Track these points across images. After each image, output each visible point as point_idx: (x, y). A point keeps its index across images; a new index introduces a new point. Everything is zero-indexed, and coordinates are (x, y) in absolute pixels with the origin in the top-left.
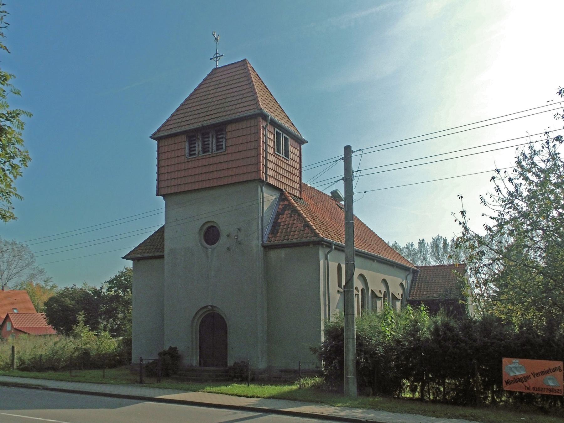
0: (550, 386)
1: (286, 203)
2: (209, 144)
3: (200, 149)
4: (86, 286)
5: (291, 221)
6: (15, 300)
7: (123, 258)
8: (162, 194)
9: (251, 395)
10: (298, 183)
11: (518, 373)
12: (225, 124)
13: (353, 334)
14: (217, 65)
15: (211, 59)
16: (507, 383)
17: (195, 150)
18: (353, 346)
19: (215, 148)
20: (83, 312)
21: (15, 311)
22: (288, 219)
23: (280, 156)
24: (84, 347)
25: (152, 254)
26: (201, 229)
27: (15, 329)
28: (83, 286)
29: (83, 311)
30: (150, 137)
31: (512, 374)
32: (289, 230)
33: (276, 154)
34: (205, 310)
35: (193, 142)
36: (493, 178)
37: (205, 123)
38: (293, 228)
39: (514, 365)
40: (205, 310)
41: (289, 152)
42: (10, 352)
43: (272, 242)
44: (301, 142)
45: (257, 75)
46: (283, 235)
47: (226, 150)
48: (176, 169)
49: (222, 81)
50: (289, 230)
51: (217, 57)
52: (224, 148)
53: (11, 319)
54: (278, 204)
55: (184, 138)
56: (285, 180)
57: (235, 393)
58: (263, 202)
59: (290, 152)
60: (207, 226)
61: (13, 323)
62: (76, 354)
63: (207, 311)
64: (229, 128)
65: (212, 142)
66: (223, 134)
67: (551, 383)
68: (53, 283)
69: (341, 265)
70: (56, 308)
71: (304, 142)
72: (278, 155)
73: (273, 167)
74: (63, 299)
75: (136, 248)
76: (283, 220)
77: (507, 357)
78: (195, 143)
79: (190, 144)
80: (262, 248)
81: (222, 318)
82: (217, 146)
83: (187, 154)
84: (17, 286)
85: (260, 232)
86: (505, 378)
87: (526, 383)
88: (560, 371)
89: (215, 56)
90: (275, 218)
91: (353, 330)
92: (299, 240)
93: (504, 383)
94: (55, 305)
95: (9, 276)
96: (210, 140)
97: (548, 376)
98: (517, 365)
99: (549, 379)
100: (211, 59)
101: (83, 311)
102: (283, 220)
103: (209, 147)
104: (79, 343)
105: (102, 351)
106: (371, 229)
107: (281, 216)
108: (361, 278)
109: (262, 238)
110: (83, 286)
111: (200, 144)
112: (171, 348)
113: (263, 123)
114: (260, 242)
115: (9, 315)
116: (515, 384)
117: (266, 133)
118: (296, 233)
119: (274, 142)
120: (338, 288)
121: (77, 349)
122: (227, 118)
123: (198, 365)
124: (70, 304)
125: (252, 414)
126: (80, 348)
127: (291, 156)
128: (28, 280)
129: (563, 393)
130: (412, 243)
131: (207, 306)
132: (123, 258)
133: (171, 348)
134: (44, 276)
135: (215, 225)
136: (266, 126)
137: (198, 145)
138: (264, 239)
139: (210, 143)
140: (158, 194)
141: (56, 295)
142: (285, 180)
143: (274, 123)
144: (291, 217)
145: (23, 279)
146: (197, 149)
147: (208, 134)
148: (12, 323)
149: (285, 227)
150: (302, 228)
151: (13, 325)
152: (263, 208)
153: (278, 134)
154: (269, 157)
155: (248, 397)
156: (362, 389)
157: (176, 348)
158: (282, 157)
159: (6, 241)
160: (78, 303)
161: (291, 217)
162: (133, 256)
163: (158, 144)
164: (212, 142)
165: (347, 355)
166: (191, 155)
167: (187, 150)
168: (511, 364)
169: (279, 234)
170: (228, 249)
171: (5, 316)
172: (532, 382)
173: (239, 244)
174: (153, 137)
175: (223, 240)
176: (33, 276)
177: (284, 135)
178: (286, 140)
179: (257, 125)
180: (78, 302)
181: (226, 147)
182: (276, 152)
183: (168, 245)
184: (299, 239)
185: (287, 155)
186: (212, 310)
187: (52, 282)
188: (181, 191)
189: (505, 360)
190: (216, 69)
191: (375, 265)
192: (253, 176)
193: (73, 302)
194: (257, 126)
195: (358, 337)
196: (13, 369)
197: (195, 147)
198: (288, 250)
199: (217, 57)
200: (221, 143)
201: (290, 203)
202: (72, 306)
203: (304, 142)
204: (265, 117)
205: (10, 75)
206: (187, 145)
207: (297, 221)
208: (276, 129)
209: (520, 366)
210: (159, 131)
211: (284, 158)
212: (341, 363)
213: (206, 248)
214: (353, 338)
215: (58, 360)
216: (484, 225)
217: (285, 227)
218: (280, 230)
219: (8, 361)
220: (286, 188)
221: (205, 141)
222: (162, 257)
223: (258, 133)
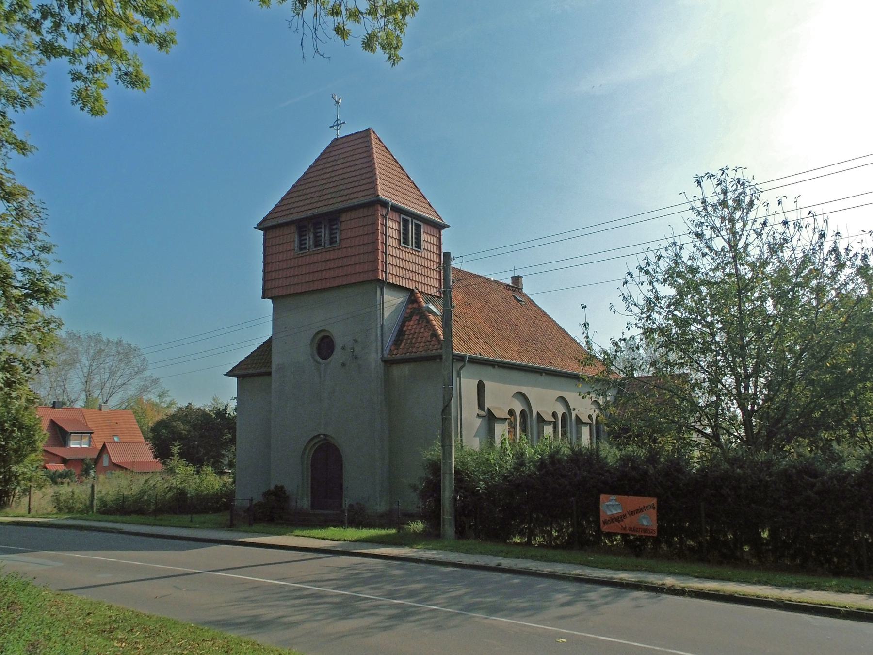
0: (643, 525)
1: (415, 305)
2: (321, 236)
3: (311, 243)
4: (216, 402)
5: (418, 330)
6: (117, 423)
7: (225, 375)
8: (270, 296)
9: (338, 538)
10: (436, 279)
11: (614, 512)
12: (340, 212)
13: (451, 470)
14: (337, 135)
15: (331, 127)
16: (605, 523)
17: (305, 243)
18: (450, 483)
19: (327, 242)
20: (177, 443)
21: (116, 439)
22: (414, 327)
23: (408, 248)
24: (179, 486)
25: (258, 371)
26: (313, 340)
27: (114, 464)
28: (213, 402)
29: (178, 441)
30: (255, 228)
31: (609, 513)
32: (413, 341)
33: (402, 246)
34: (316, 440)
35: (304, 233)
36: (626, 283)
37: (316, 211)
38: (419, 338)
39: (611, 503)
40: (316, 440)
41: (422, 241)
42: (90, 490)
43: (394, 356)
44: (439, 227)
45: (385, 147)
47: (340, 244)
48: (285, 266)
49: (341, 156)
50: (413, 341)
51: (338, 125)
52: (338, 241)
53: (109, 449)
54: (406, 308)
55: (293, 229)
56: (417, 278)
57: (323, 537)
58: (383, 308)
59: (424, 241)
60: (320, 336)
61: (111, 456)
62: (170, 494)
63: (319, 441)
64: (344, 217)
66: (336, 224)
67: (645, 523)
68: (170, 399)
69: (484, 382)
70: (166, 435)
71: (444, 226)
72: (405, 247)
73: (398, 262)
74: (174, 424)
75: (241, 362)
76: (409, 328)
77: (605, 494)
78: (305, 235)
79: (300, 236)
80: (382, 364)
81: (337, 450)
82: (331, 239)
83: (296, 249)
84: (122, 403)
85: (379, 344)
86: (602, 519)
87: (622, 523)
88: (654, 508)
89: (336, 124)
90: (401, 326)
91: (451, 463)
92: (424, 354)
93: (602, 524)
94: (164, 431)
95: (112, 389)
96: (323, 231)
97: (642, 515)
98: (614, 502)
99: (644, 518)
100: (331, 127)
101: (178, 441)
102: (409, 328)
103: (321, 240)
104: (176, 482)
105: (202, 491)
106: (566, 330)
107: (407, 322)
108: (521, 398)
109: (382, 352)
110: (213, 402)
111: (312, 236)
112: (276, 487)
113: (382, 211)
114: (380, 355)
115: (106, 444)
116: (612, 525)
117: (386, 223)
118: (422, 344)
119: (399, 231)
120: (476, 411)
121: (171, 489)
122: (340, 206)
123: (310, 508)
124: (184, 430)
125: (315, 555)
126: (174, 488)
127: (424, 245)
128: (137, 394)
129: (656, 534)
131: (320, 435)
132: (225, 375)
133: (276, 487)
134: (158, 389)
136: (387, 214)
137: (310, 238)
138: (384, 352)
139: (323, 235)
140: (264, 297)
141: (165, 417)
142: (417, 278)
144: (418, 324)
145: (130, 393)
146: (307, 242)
148: (110, 456)
149: (411, 336)
150: (429, 339)
151: (111, 459)
152: (383, 314)
153: (406, 222)
154: (390, 251)
155: (335, 541)
156: (461, 533)
157: (282, 487)
158: (412, 249)
159: (109, 340)
160: (194, 429)
161: (418, 324)
162: (236, 372)
163: (265, 235)
165: (444, 492)
166: (301, 249)
167: (297, 244)
168: (607, 502)
169: (402, 345)
170: (343, 365)
171: (102, 446)
172: (627, 522)
173: (355, 358)
174: (259, 227)
175: (338, 355)
176: (144, 389)
177: (415, 221)
178: (418, 227)
179: (374, 215)
180: (194, 427)
181: (340, 240)
182: (402, 244)
183: (276, 360)
184: (403, 355)
185: (418, 245)
186: (325, 439)
187: (169, 396)
188: (298, 292)
189: (602, 497)
190: (336, 139)
191: (543, 379)
192: (369, 276)
193: (187, 427)
194: (374, 215)
195: (457, 472)
196: (93, 512)
197: (306, 239)
198: (412, 365)
199: (338, 124)
201: (419, 306)
202: (186, 433)
203: (444, 226)
204: (384, 204)
205: (54, 245)
206: (296, 236)
207: (425, 330)
208: (402, 216)
209: (617, 503)
210: (265, 219)
211: (415, 250)
212: (438, 501)
213: (319, 363)
214: (451, 473)
215: (148, 502)
216: (611, 339)
217: (411, 336)
218: (404, 341)
219: (88, 503)
220: (417, 287)
221: (317, 233)
222: (269, 374)
223: (375, 224)
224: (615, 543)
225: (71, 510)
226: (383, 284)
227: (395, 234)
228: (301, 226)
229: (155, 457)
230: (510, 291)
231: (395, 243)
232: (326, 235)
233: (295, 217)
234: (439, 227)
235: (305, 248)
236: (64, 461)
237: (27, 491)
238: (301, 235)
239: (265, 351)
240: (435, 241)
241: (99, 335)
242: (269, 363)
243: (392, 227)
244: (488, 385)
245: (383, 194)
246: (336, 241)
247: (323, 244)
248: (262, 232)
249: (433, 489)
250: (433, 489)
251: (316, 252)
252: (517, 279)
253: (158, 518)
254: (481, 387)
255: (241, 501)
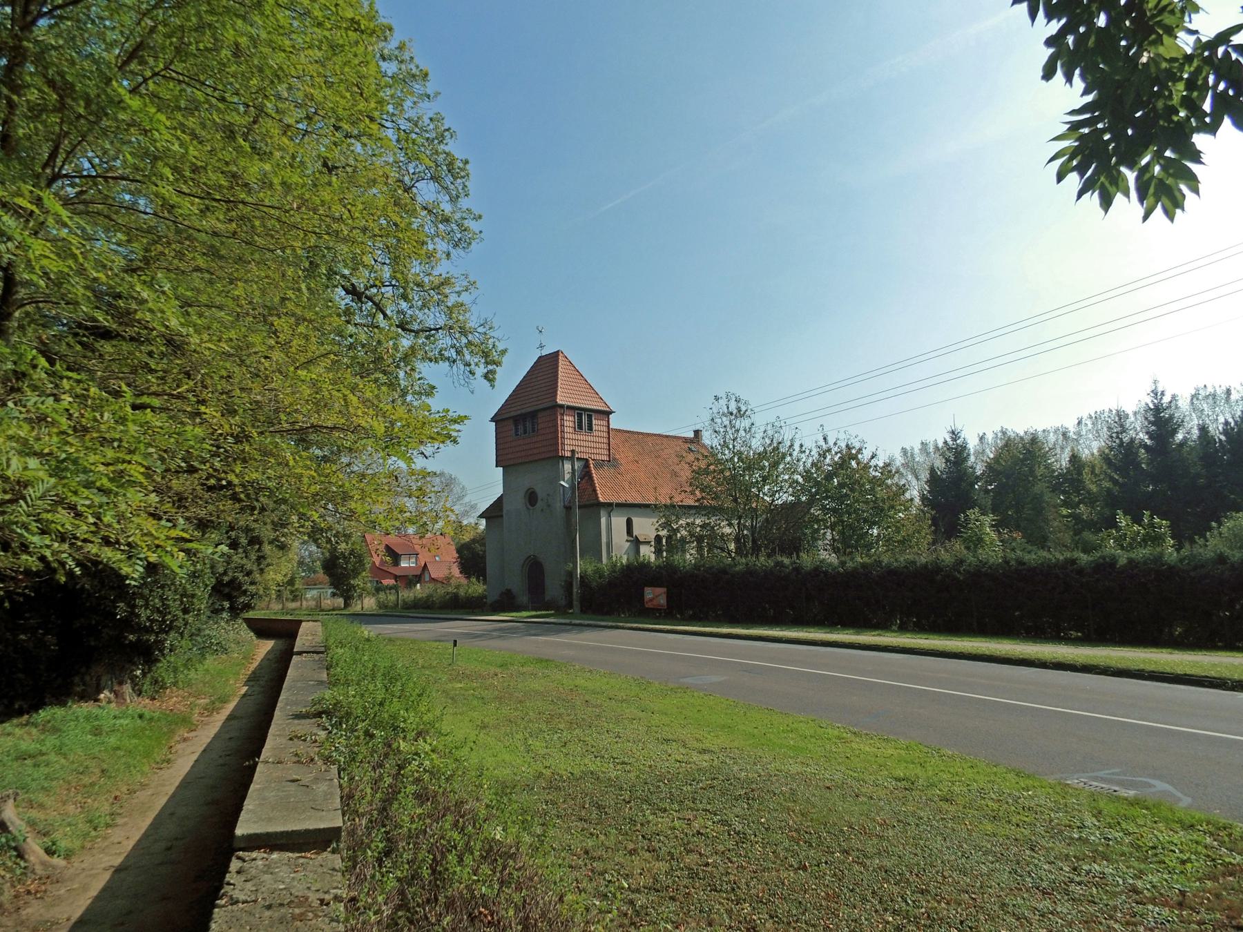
37: (523, 411)
44: (607, 413)
71: (611, 412)
120: (625, 537)
127: (594, 427)
153: (580, 416)
174: (492, 420)
175: (539, 504)
185: (590, 428)
199: (541, 347)
203: (611, 412)
222: (502, 516)
225: (386, 607)
227: (571, 424)
228: (517, 420)
229: (461, 572)
231: (571, 430)
233: (513, 414)
234: (607, 413)
236: (396, 577)
237: (360, 596)
238: (516, 426)
239: (499, 503)
240: (605, 423)
242: (501, 510)
243: (569, 421)
244: (635, 520)
249: (569, 586)
250: (569, 586)
254: (629, 523)
255: (489, 600)
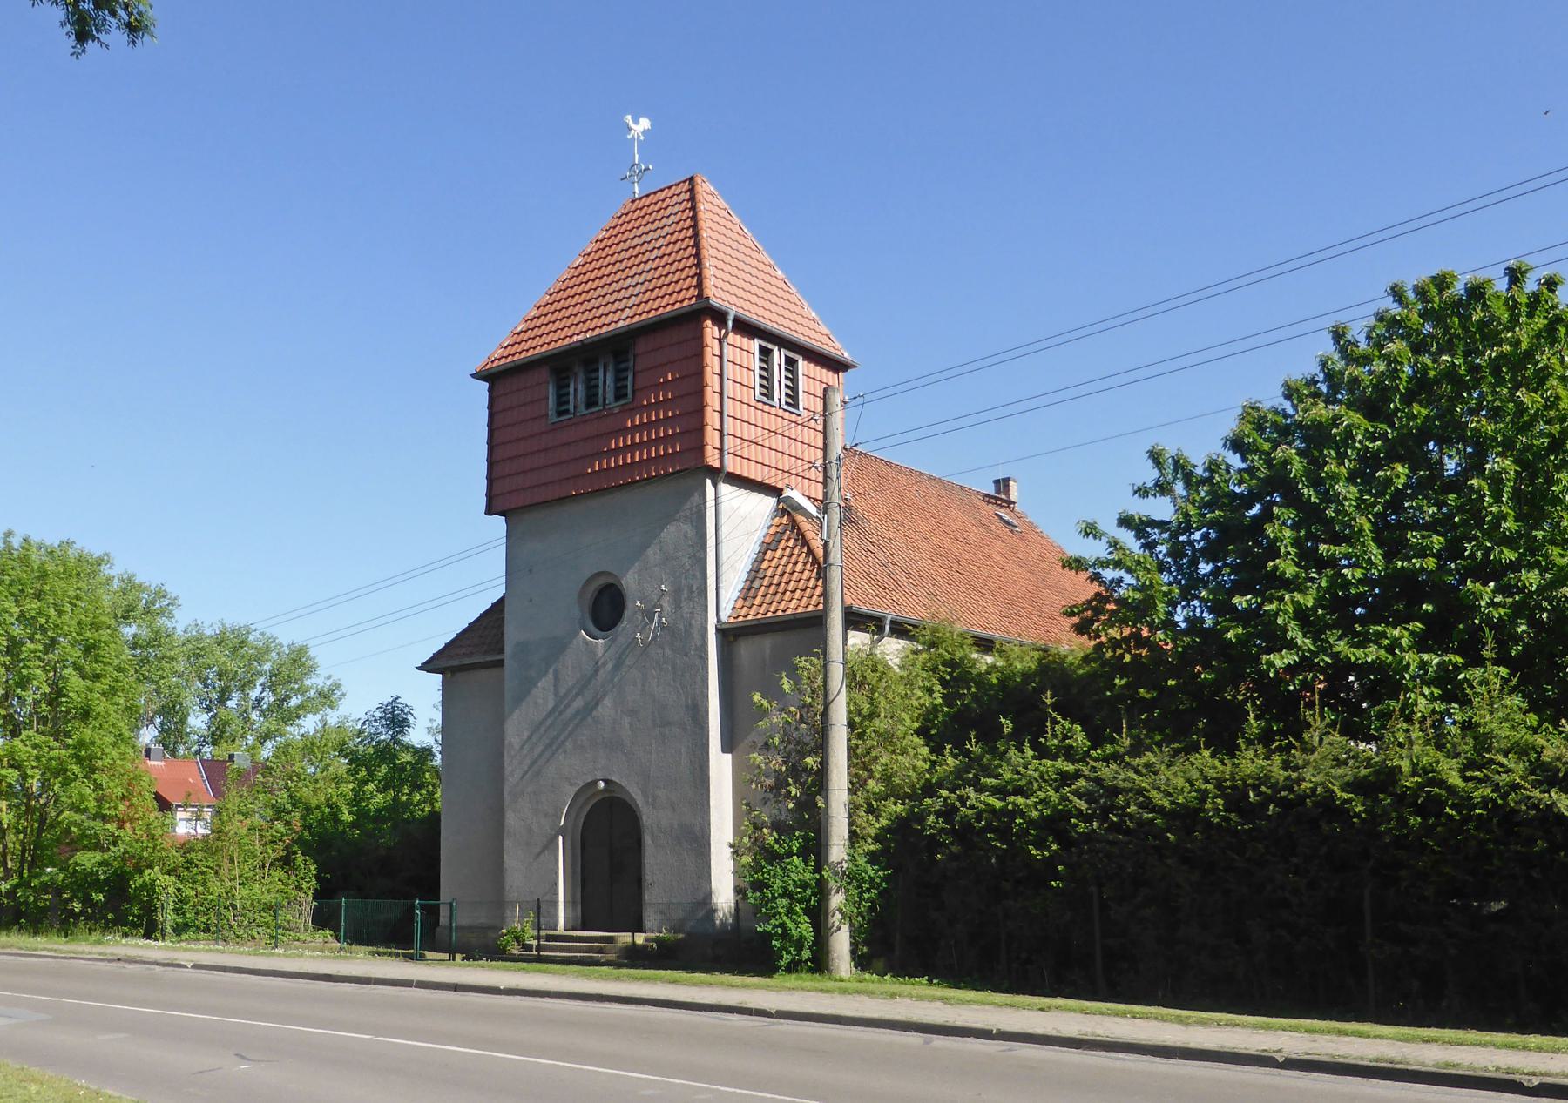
7: (418, 668)
8: (500, 509)
17: (568, 402)
19: (610, 396)
46: (784, 580)
55: (544, 373)
60: (602, 581)
64: (642, 345)
65: (606, 380)
82: (617, 389)
111: (580, 388)
113: (711, 331)
130: (1551, 284)
135: (611, 581)
139: (601, 384)
140: (489, 512)
143: (746, 328)
147: (596, 361)
153: (765, 353)
162: (444, 663)
163: (491, 390)
164: (606, 380)
166: (560, 413)
178: (791, 363)
181: (634, 392)
183: (513, 634)
185: (793, 400)
200: (625, 383)
204: (719, 317)
222: (500, 664)
224: (933, 732)
226: (718, 475)
230: (990, 506)
232: (608, 383)
235: (567, 412)
241: (134, 576)
245: (717, 294)
246: (626, 395)
247: (601, 401)
248: (486, 385)
251: (588, 417)
252: (1003, 484)
253: (183, 937)
